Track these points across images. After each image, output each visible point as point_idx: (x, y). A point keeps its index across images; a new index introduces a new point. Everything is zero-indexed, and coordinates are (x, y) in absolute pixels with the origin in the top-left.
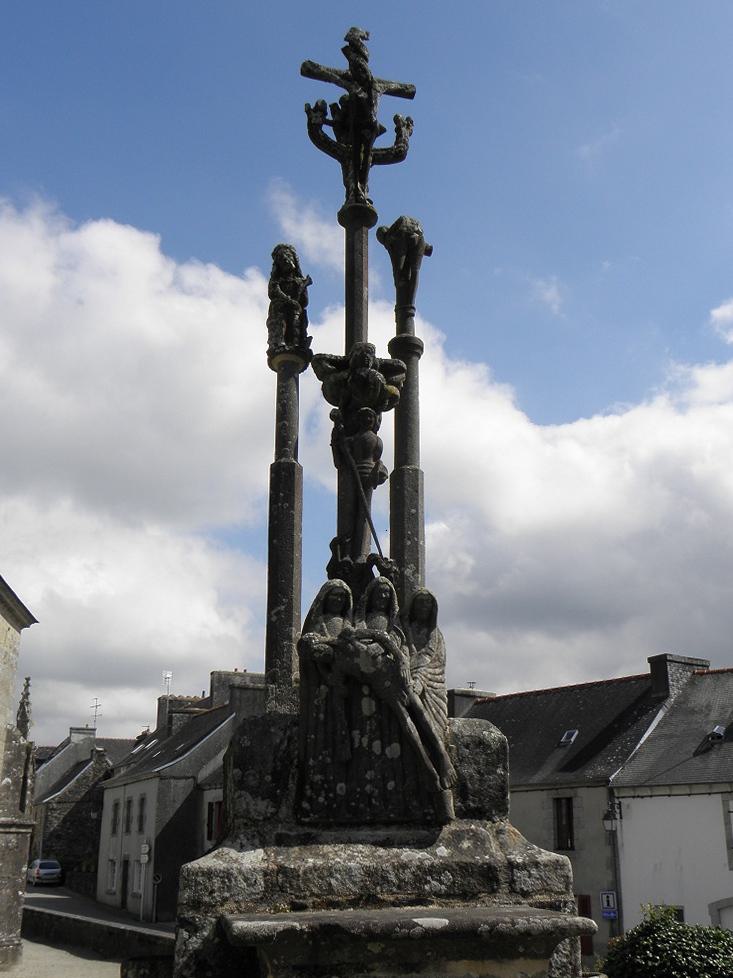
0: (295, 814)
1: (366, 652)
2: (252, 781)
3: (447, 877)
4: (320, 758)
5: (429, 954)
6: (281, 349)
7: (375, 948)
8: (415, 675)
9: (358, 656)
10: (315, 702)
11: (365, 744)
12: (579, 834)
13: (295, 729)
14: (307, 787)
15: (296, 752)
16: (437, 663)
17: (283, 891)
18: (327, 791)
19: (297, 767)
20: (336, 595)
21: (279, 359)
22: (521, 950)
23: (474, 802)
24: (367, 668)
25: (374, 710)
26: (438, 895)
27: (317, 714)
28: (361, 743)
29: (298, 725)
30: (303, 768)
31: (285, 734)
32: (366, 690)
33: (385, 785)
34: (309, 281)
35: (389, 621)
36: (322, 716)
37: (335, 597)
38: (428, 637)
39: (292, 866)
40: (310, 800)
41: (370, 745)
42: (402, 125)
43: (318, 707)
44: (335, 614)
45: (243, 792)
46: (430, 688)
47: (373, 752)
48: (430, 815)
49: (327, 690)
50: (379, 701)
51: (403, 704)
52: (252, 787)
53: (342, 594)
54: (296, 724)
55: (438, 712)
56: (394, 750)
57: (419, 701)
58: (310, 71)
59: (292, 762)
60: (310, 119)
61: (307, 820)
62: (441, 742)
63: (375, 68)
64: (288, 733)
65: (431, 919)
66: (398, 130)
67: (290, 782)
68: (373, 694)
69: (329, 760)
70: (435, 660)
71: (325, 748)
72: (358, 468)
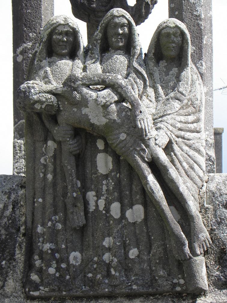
0: (24, 287)
1: (96, 100)
4: (50, 224)
8: (159, 125)
11: (101, 208)
13: (21, 192)
14: (36, 257)
15: (23, 219)
16: (191, 109)
18: (59, 262)
19: (24, 235)
20: (60, 34)
25: (111, 166)
27: (45, 174)
28: (97, 206)
29: (25, 187)
30: (31, 238)
31: (9, 198)
32: (100, 145)
33: (126, 254)
35: (129, 62)
36: (50, 177)
37: (60, 37)
38: (178, 79)
40: (40, 272)
41: (107, 209)
43: (45, 166)
44: (62, 56)
46: (180, 139)
48: (179, 284)
49: (56, 146)
50: (117, 158)
51: (143, 159)
53: (67, 33)
54: (22, 187)
55: (192, 168)
56: (136, 214)
59: (18, 230)
61: (36, 294)
64: (13, 196)
67: (17, 252)
68: (108, 149)
69: (60, 226)
70: (187, 106)
71: (55, 213)
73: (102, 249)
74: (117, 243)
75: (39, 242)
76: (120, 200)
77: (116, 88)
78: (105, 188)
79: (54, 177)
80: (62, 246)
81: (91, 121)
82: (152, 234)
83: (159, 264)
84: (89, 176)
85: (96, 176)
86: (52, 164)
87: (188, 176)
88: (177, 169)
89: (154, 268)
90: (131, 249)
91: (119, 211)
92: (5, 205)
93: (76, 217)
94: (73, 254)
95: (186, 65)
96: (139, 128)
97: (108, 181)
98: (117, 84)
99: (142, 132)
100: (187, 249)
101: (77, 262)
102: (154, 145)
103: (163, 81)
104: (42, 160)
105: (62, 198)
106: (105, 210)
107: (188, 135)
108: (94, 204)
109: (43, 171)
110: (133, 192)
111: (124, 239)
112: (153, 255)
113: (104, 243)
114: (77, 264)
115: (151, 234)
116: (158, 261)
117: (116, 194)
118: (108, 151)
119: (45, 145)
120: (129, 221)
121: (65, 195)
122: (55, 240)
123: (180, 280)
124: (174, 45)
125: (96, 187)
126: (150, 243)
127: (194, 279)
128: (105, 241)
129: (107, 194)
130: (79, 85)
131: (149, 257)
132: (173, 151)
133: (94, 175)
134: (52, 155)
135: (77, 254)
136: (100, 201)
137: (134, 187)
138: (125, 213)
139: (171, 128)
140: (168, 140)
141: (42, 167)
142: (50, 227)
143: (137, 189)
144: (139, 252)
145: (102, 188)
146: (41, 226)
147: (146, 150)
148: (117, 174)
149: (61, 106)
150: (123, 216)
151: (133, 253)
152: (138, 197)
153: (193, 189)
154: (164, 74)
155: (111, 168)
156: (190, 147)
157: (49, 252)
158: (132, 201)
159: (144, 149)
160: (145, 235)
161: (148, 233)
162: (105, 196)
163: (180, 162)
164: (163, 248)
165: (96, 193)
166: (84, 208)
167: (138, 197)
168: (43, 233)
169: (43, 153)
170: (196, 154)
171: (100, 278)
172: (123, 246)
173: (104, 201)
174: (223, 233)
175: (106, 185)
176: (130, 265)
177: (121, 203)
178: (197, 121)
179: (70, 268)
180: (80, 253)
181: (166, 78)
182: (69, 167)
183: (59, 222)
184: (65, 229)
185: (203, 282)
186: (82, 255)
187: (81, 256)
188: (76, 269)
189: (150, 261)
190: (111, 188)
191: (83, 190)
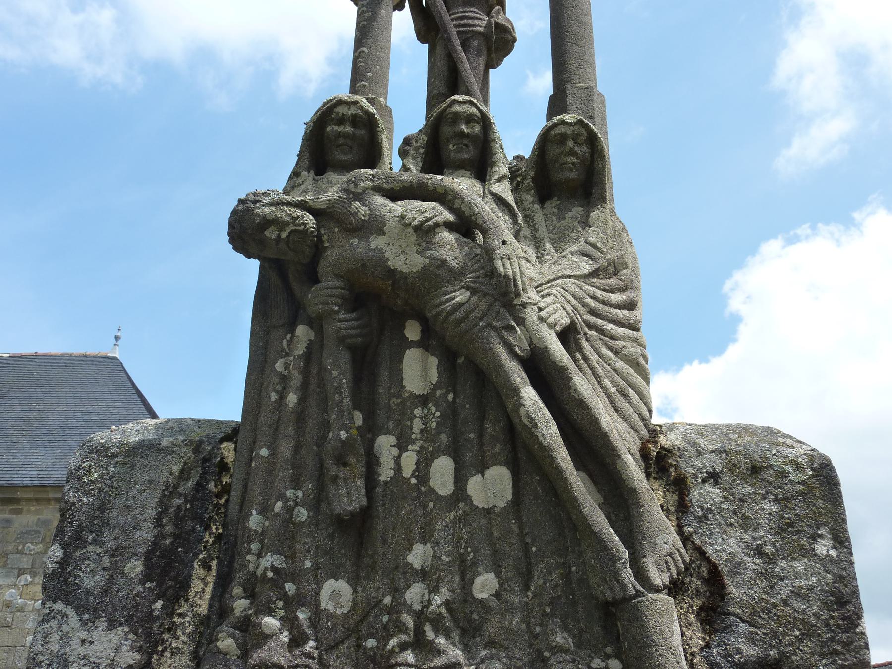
2: (90, 580)
9: (381, 232)
14: (237, 590)
23: (751, 639)
24: (406, 260)
27: (282, 397)
28: (398, 468)
32: (413, 332)
33: (467, 585)
34: (838, 242)
36: (292, 399)
41: (422, 471)
43: (284, 379)
45: (59, 606)
46: (594, 333)
47: (432, 491)
50: (449, 358)
52: (88, 593)
53: (355, 121)
55: (626, 396)
56: (492, 487)
57: (557, 348)
62: (629, 459)
68: (430, 340)
69: (303, 514)
72: (456, 26)
73: (405, 573)
74: (443, 557)
75: (249, 552)
76: (456, 455)
77: (450, 201)
78: (417, 425)
79: (302, 400)
80: (303, 565)
81: (389, 263)
82: (534, 540)
83: (552, 615)
84: (383, 401)
85: (399, 401)
86: (301, 373)
87: (617, 410)
89: (538, 629)
90: (479, 574)
91: (450, 479)
92: (336, 594)
93: (343, 491)
94: (330, 585)
96: (500, 275)
97: (426, 411)
98: (453, 191)
99: (508, 286)
101: (339, 605)
102: (535, 319)
103: (554, 229)
104: (279, 366)
105: (315, 448)
106: (417, 477)
108: (392, 464)
109: (279, 387)
110: (487, 437)
111: (462, 551)
112: (534, 596)
113: (410, 558)
114: (339, 612)
115: (529, 540)
116: (548, 610)
117: (444, 437)
118: (429, 345)
119: (289, 336)
120: (475, 503)
121: (322, 439)
122: (290, 547)
123: (610, 661)
124: (574, 159)
125: (398, 425)
126: (529, 564)
127: (651, 656)
128: (413, 552)
129: (424, 441)
130: (367, 189)
131: (525, 599)
133: (394, 400)
134: (301, 353)
135: (342, 586)
136: (405, 455)
137: (488, 425)
138: (466, 484)
140: (567, 321)
141: (277, 380)
142: (278, 515)
143: (494, 430)
144: (501, 584)
145: (412, 424)
146: (259, 513)
147: (518, 328)
148: (448, 392)
149: (325, 238)
150: (460, 493)
151: (483, 586)
152: (498, 448)
153: (631, 440)
154: (554, 218)
155: (435, 379)
156: (616, 352)
157: (270, 574)
158: (483, 456)
159: (513, 328)
160: (515, 540)
161: (522, 536)
162: (419, 443)
163: (595, 377)
164: (562, 574)
165: (398, 440)
166: (364, 469)
167: (497, 449)
168: (262, 531)
169: (284, 350)
171: (393, 647)
172: (460, 567)
173: (414, 455)
174: (711, 544)
175: (421, 418)
176: (475, 617)
177: (456, 462)
179: (319, 620)
180: (351, 585)
181: (558, 224)
182: (335, 373)
183: (303, 504)
184: (314, 522)
185: (678, 663)
186: (355, 591)
187: (352, 592)
188: (335, 625)
189: (527, 609)
190: (434, 424)
191: (369, 436)
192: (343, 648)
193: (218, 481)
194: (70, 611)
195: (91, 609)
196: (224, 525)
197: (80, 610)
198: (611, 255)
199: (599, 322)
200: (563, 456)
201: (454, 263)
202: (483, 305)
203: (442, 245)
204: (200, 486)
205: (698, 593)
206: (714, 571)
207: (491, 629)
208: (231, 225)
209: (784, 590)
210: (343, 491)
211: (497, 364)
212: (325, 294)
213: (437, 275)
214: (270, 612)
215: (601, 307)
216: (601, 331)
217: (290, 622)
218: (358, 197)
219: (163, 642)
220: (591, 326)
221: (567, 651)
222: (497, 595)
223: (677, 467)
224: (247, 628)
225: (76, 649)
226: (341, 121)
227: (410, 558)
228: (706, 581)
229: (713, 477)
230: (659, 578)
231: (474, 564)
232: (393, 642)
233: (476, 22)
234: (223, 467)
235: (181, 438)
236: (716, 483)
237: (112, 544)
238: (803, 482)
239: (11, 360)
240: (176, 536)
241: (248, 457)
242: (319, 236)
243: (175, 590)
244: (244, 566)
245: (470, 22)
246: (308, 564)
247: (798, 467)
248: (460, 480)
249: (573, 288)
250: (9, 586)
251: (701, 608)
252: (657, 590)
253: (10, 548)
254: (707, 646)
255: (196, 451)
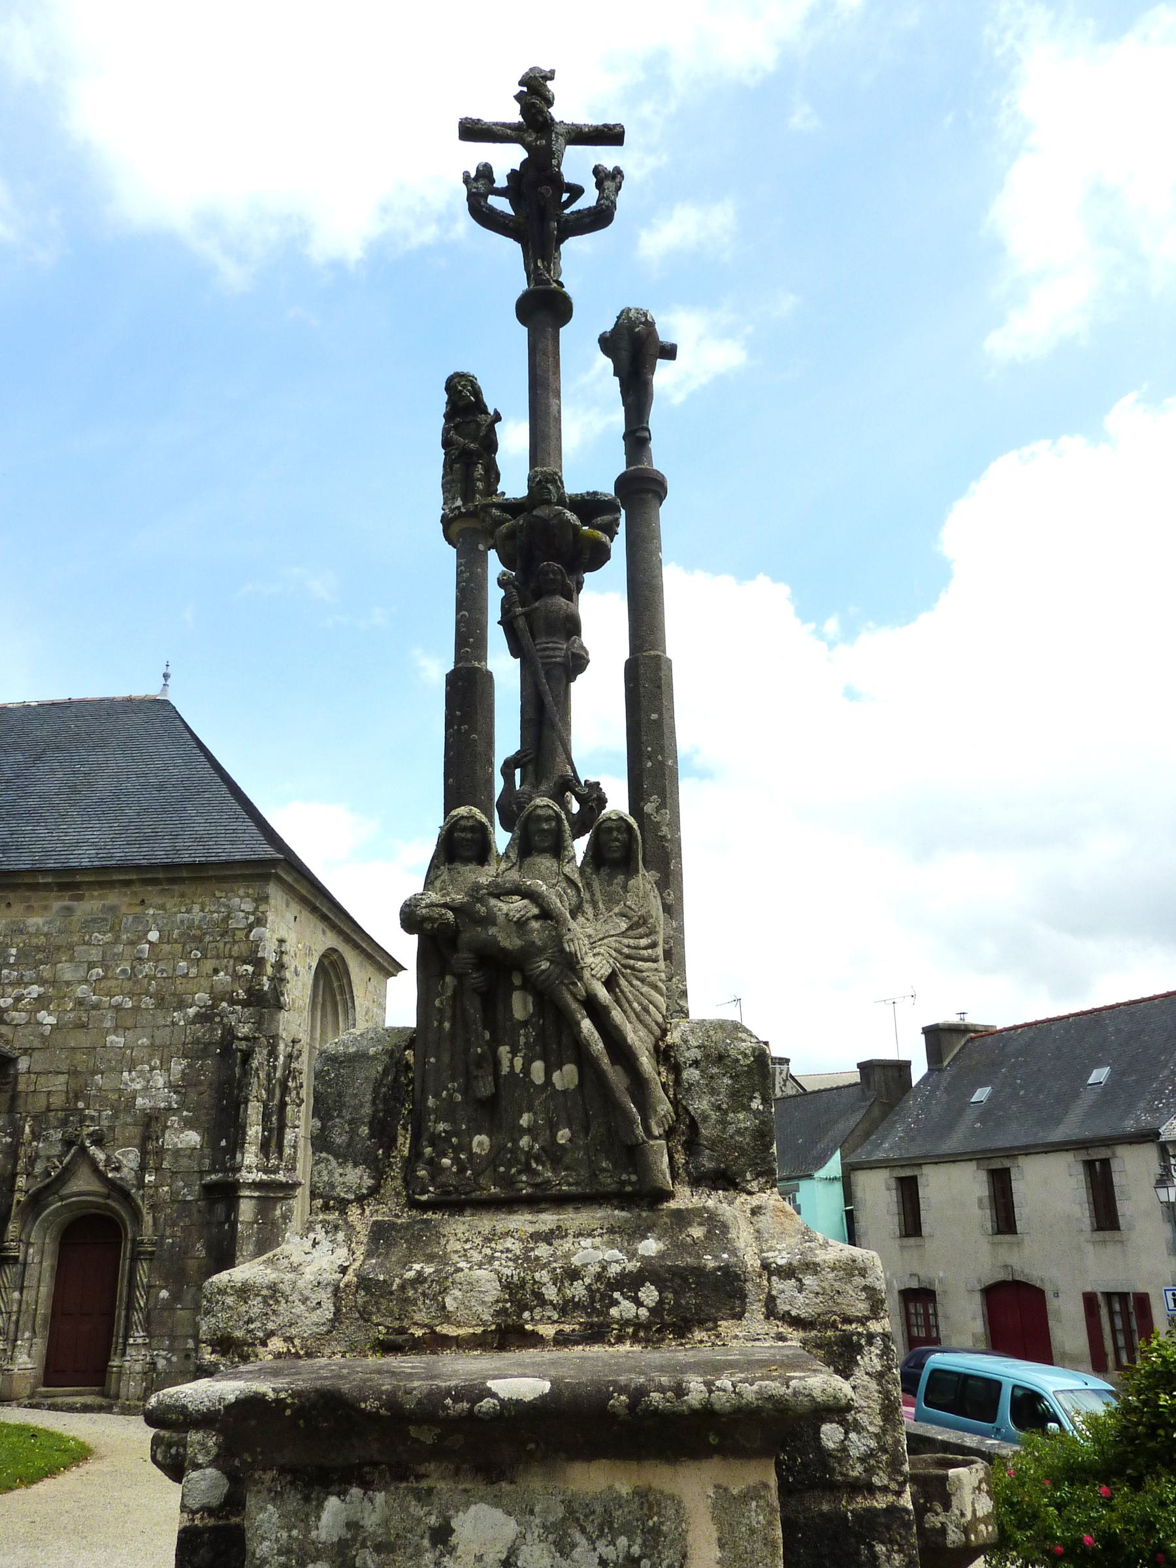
2: (340, 1140)
3: (649, 1294)
5: (532, 1446)
6: (457, 512)
7: (427, 1436)
9: (494, 924)
10: (437, 1003)
12: (1124, 1208)
17: (366, 1321)
21: (455, 528)
22: (713, 1440)
23: (711, 1159)
24: (510, 942)
25: (531, 1009)
26: (638, 1325)
27: (441, 1023)
28: (512, 1066)
32: (517, 981)
33: (554, 1136)
34: (497, 417)
36: (447, 1025)
39: (381, 1278)
41: (526, 1069)
42: (608, 179)
43: (440, 1010)
45: (324, 1155)
47: (532, 1082)
48: (630, 1183)
51: (574, 996)
52: (339, 1146)
53: (472, 829)
56: (566, 1077)
57: (602, 993)
58: (472, 131)
60: (469, 190)
61: (425, 1198)
63: (566, 110)
65: (519, 1381)
66: (599, 185)
68: (531, 985)
69: (459, 1097)
72: (541, 658)
76: (544, 1058)
79: (452, 1026)
88: (625, 1012)
92: (481, 1143)
93: (481, 1084)
94: (477, 1138)
95: (637, 871)
100: (640, 1131)
104: (437, 1003)
107: (639, 964)
113: (521, 1122)
121: (467, 1050)
132: (619, 986)
139: (614, 954)
140: (610, 971)
156: (643, 981)
170: (653, 992)
178: (653, 945)
182: (472, 1011)
183: (457, 1091)
186: (491, 1140)
192: (487, 1173)
193: (406, 1076)
194: (331, 1158)
195: (345, 1156)
196: (413, 1103)
197: (336, 1157)
198: (643, 912)
199: (632, 962)
200: (605, 1061)
201: (539, 943)
202: (557, 971)
203: (532, 931)
204: (395, 1080)
205: (683, 1134)
206: (692, 1119)
207: (567, 1160)
208: (402, 912)
209: (731, 1130)
210: (481, 1084)
211: (567, 1006)
212: (463, 958)
213: (529, 952)
214: (445, 1156)
215: (633, 952)
216: (633, 968)
217: (456, 1160)
218: (480, 900)
219: (386, 1173)
220: (625, 967)
221: (608, 1171)
222: (570, 1140)
223: (675, 1057)
224: (433, 1164)
225: (337, 1179)
226: (464, 829)
227: (521, 1122)
228: (688, 1127)
229: (696, 1063)
230: (656, 1131)
231: (557, 1123)
232: (513, 1170)
233: (557, 653)
234: (408, 1067)
235: (380, 1048)
236: (697, 1068)
237: (348, 1117)
238: (748, 1066)
239: (40, 710)
240: (385, 1111)
241: (421, 1059)
242: (457, 926)
243: (390, 1144)
244: (428, 1128)
245: (552, 653)
246: (464, 1127)
247: (745, 1056)
248: (548, 1074)
249: (614, 945)
250: (80, 982)
251: (685, 1142)
252: (656, 1138)
253: (75, 939)
254: (687, 1163)
255: (391, 1057)
